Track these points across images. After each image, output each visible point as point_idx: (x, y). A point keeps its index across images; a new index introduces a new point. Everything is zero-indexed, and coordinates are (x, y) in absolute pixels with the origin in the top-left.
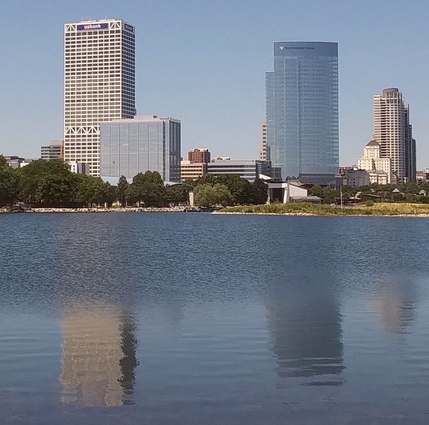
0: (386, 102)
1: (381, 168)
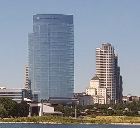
0: (103, 52)
1: (101, 94)
